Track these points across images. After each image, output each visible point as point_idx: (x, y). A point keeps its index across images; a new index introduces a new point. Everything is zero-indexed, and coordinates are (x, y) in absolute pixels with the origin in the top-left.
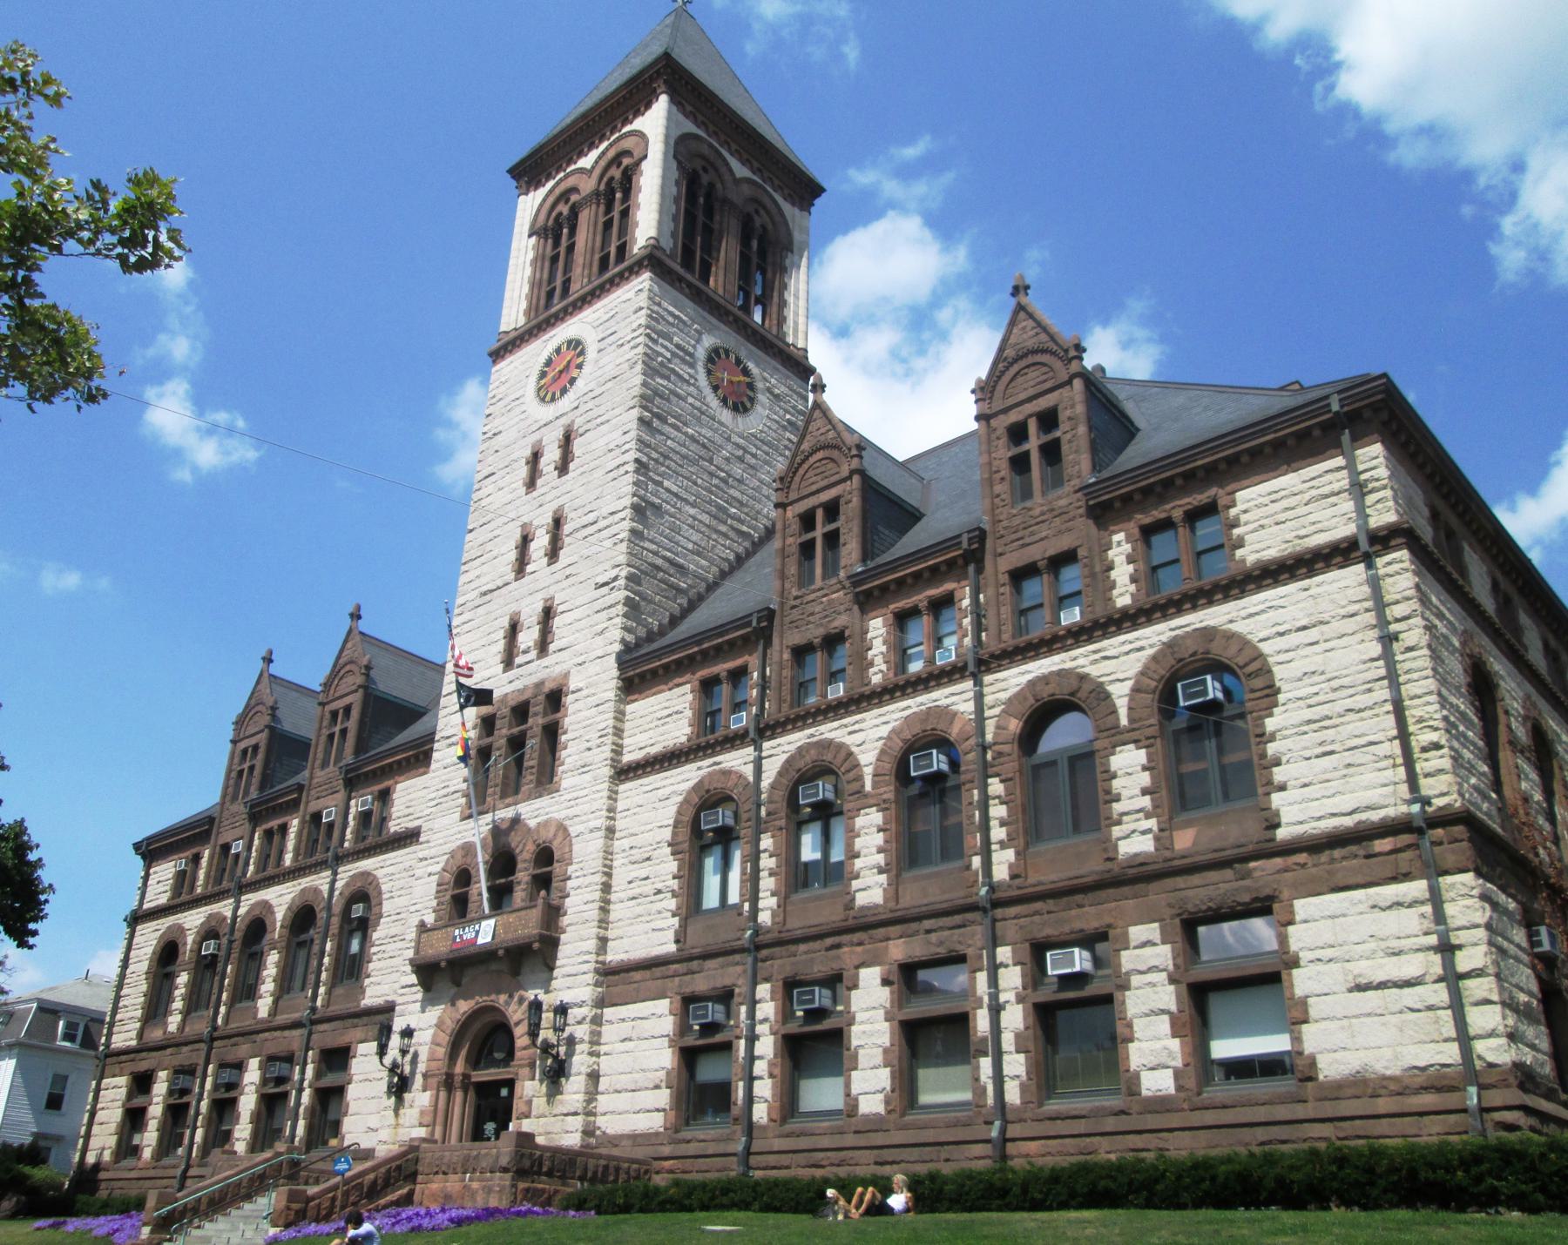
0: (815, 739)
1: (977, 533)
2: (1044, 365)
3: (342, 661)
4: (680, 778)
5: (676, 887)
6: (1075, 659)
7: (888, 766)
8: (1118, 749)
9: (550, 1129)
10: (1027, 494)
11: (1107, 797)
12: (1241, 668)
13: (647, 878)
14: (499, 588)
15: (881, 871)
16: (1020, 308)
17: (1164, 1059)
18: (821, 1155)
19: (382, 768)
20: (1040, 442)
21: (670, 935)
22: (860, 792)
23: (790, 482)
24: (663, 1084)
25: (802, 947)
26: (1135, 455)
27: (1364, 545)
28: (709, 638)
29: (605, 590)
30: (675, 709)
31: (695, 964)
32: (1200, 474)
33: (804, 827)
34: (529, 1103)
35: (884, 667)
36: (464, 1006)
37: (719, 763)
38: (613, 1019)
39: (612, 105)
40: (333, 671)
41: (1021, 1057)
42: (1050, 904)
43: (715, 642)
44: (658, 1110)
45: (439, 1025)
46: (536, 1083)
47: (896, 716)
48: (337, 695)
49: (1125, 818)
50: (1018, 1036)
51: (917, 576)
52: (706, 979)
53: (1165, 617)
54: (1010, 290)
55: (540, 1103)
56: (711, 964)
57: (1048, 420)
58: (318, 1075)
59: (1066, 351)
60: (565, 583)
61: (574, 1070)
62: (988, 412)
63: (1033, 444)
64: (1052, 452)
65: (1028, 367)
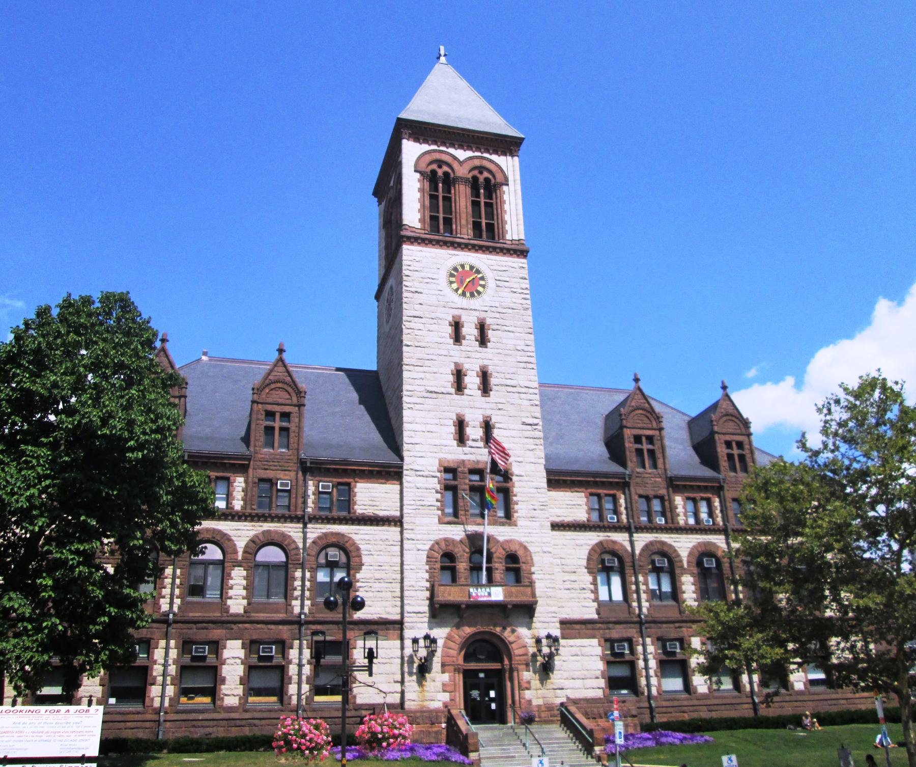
2: (287, 391)
3: (271, 377)
7: (694, 561)
8: (236, 568)
9: (546, 696)
13: (576, 581)
14: (443, 393)
15: (244, 598)
17: (801, 679)
18: (686, 708)
21: (594, 611)
22: (682, 567)
25: (665, 625)
28: (600, 477)
29: (529, 427)
31: (611, 625)
32: (227, 465)
34: (529, 682)
35: (313, 506)
36: (468, 630)
38: (565, 644)
44: (599, 688)
45: (449, 638)
51: (699, 487)
52: (617, 632)
53: (652, 532)
55: (535, 683)
56: (618, 626)
59: (301, 392)
61: (556, 668)
65: (280, 388)
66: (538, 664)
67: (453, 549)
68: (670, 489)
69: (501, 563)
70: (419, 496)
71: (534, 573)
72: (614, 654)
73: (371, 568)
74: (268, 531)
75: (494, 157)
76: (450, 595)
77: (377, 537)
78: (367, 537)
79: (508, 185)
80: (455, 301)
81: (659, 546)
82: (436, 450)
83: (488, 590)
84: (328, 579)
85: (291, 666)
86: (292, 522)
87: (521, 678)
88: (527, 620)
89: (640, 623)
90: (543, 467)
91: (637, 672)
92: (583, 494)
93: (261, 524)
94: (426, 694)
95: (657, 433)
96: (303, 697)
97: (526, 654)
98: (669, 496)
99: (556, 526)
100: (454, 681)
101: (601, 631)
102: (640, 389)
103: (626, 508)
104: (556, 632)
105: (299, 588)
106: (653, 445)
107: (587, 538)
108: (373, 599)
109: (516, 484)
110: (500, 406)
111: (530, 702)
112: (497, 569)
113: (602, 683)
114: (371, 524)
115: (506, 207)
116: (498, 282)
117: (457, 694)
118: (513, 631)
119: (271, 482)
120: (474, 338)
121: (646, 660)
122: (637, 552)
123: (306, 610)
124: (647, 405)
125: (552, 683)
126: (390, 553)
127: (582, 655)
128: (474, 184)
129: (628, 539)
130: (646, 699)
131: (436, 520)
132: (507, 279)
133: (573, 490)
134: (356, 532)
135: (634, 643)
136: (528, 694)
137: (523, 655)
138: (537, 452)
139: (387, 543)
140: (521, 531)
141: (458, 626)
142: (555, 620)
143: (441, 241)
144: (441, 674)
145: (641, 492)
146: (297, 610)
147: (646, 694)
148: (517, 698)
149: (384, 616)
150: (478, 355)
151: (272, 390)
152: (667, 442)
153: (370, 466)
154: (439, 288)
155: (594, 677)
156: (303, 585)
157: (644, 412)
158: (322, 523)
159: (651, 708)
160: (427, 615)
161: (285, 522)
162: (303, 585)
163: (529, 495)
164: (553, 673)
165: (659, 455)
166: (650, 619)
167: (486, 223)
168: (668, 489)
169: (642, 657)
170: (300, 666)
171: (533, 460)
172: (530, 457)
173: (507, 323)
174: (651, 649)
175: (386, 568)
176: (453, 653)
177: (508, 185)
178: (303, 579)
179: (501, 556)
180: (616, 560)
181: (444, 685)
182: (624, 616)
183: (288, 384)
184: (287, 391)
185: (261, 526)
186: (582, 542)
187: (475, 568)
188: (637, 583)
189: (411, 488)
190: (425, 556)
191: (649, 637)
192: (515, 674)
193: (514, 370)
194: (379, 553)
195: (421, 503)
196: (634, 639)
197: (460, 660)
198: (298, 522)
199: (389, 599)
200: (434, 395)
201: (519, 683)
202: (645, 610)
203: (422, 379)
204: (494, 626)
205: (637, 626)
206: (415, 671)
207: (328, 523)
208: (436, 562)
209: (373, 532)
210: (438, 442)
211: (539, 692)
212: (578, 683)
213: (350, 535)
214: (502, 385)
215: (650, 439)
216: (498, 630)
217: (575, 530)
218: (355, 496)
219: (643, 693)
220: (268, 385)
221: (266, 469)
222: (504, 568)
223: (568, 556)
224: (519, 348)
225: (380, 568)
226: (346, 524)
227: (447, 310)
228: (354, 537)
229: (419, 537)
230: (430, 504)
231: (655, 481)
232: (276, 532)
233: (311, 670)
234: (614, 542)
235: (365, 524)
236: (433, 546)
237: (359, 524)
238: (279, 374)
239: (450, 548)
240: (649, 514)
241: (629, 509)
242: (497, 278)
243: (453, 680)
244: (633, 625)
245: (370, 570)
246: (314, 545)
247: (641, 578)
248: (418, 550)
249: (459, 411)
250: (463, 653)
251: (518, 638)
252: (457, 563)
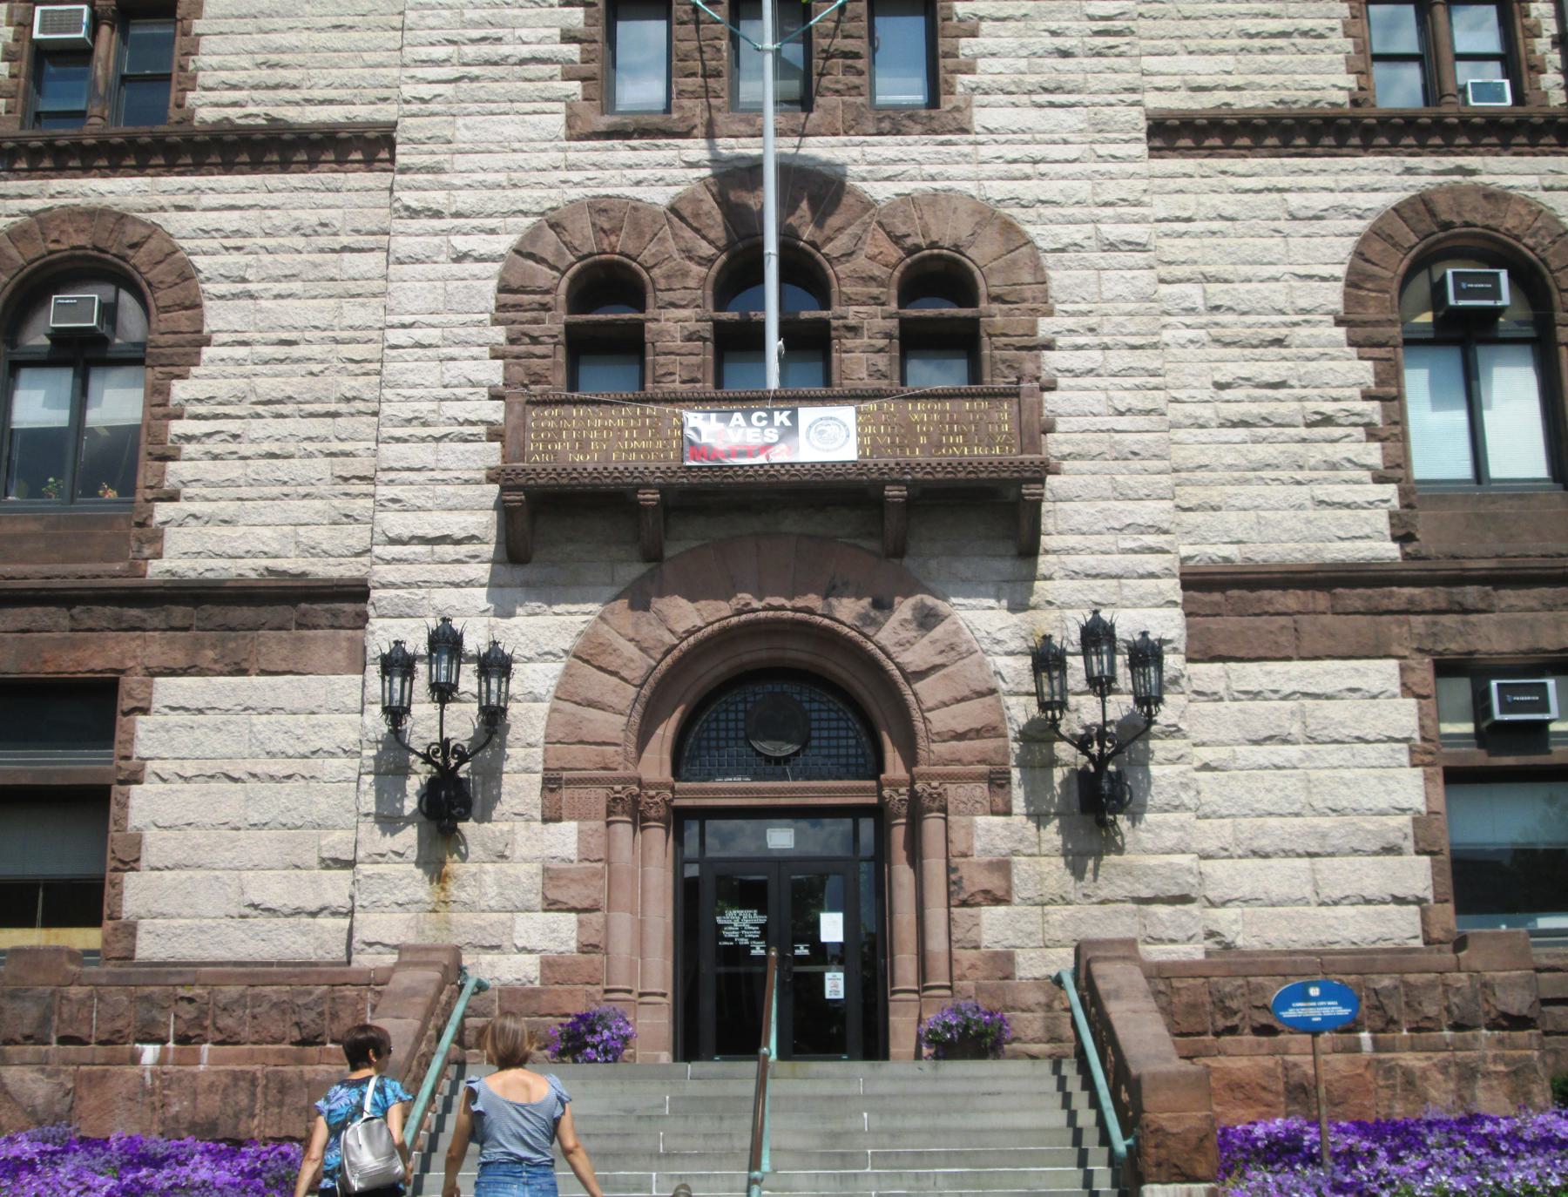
4: (1348, 180)
5: (1377, 418)
6: (638, 183)
12: (648, 270)
21: (1380, 519)
24: (1409, 845)
30: (1307, 24)
31: (1471, 594)
37: (1473, 172)
44: (1400, 901)
49: (1066, 465)
56: (1509, 596)
209: (262, 198)
228: (174, 223)
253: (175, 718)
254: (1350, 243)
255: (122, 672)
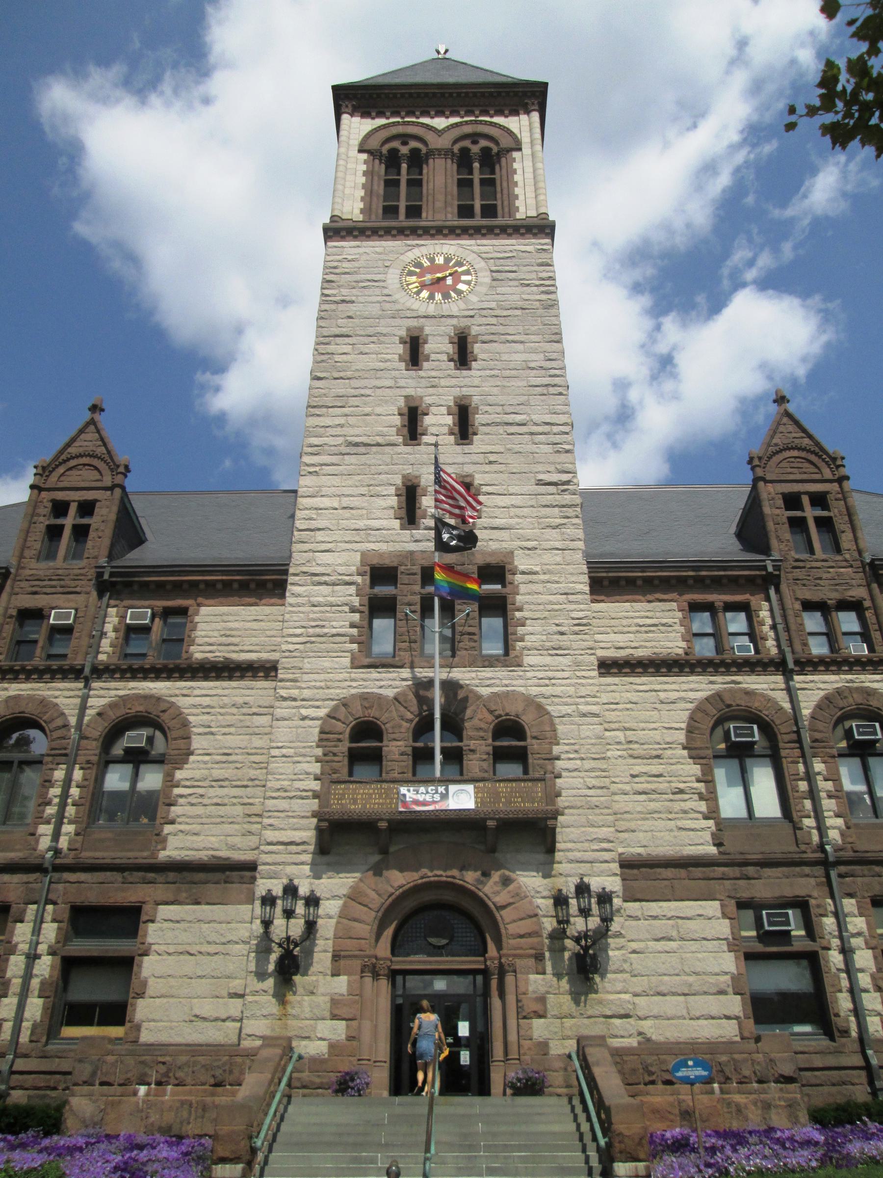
0: (855, 685)
1: (3, 571)
2: (96, 468)
3: (72, 450)
10: (51, 555)
11: (167, 801)
12: (384, 724)
14: (379, 445)
16: (92, 422)
19: (206, 583)
20: (75, 523)
23: (51, 472)
24: (730, 990)
26: (136, 557)
27: (87, 671)
28: (709, 568)
31: (751, 870)
32: (185, 586)
33: (111, 766)
34: (542, 1000)
35: (109, 650)
37: (739, 683)
39: (467, 93)
40: (57, 457)
41: (40, 1002)
42: (117, 876)
43: (716, 573)
44: (728, 1018)
45: (354, 896)
46: (549, 977)
47: (113, 693)
48: (61, 485)
49: (566, 811)
50: (42, 983)
54: (90, 405)
56: (768, 872)
57: (87, 508)
58: (64, 938)
59: (118, 466)
60: (487, 468)
61: (612, 966)
62: (42, 486)
63: (69, 521)
64: (81, 533)
65: (85, 465)
66: (567, 955)
67: (377, 715)
68: (875, 586)
69: (483, 738)
70: (314, 620)
71: (558, 758)
72: (764, 937)
73: (207, 758)
74: (17, 698)
75: (499, 120)
76: (355, 802)
77: (226, 700)
78: (206, 701)
79: (520, 149)
80: (414, 307)
81: (858, 698)
82: (357, 539)
83: (441, 789)
84: (125, 786)
85: (13, 958)
86: (64, 678)
87: (522, 989)
88: (541, 857)
89: (826, 864)
90: (579, 556)
91: (827, 980)
92: (674, 605)
93: (6, 685)
94: (292, 1023)
95: (835, 486)
96: (26, 1025)
97: (536, 934)
98: (873, 599)
99: (607, 667)
100: (360, 995)
101: (727, 883)
102: (788, 414)
103: (774, 627)
104: (613, 884)
105: (56, 800)
106: (829, 510)
107: (685, 687)
108: (204, 820)
109: (523, 588)
110: (492, 458)
111: (544, 1046)
112: (473, 751)
113: (735, 1005)
114: (218, 678)
115: (517, 178)
116: (494, 274)
117: (367, 1025)
118: (506, 882)
119: (37, 615)
120: (445, 357)
121: (846, 951)
122: (806, 712)
123: (63, 843)
124: (807, 441)
125: (600, 1002)
126: (250, 731)
127: (682, 939)
128: (464, 160)
129: (783, 686)
130: (856, 1046)
131: (346, 661)
132: (514, 269)
133: (650, 597)
134: (185, 692)
135: (814, 911)
136: (539, 1028)
137: (529, 935)
138: (570, 531)
139: (245, 710)
140: (529, 674)
141: (378, 870)
142: (607, 856)
143: (394, 228)
144: (329, 978)
145: (808, 595)
146: (45, 843)
147: (854, 1034)
148: (512, 1037)
149: (224, 853)
150: (454, 382)
151: (70, 469)
152: (857, 501)
153: (223, 573)
154: (386, 292)
155: (714, 990)
156: (65, 795)
157: (803, 454)
158: (122, 678)
159: (868, 1067)
160: (311, 848)
161: (53, 679)
162: (65, 795)
163: (550, 607)
164: (603, 976)
165: (841, 524)
166: (848, 854)
167: (482, 206)
168: (868, 585)
169: (836, 942)
170: (32, 957)
171: (558, 545)
172: (553, 538)
173: (510, 330)
174: (857, 923)
175: (239, 758)
176: (365, 930)
177: (520, 149)
178: (67, 783)
179: (483, 725)
180: (755, 727)
181: (334, 1002)
182: (783, 846)
183: (99, 458)
184: (96, 468)
185: (6, 689)
186: (674, 695)
187: (423, 756)
188: (809, 777)
189: (298, 605)
190: (317, 730)
191: (850, 895)
192: (509, 979)
193: (523, 399)
194: (226, 730)
195: (318, 631)
196: (812, 902)
197: (384, 948)
198: (77, 679)
199: (239, 819)
200: (362, 449)
201: (518, 1001)
202: (834, 835)
203: (341, 426)
204: (463, 868)
205: (819, 870)
206: (271, 967)
207: (134, 678)
208: (339, 740)
210: (361, 524)
211: (568, 1022)
212: (672, 1005)
213: (173, 699)
214: (497, 424)
215: (819, 500)
216: (470, 877)
217: (657, 673)
218: (194, 629)
219: (846, 1032)
220: (65, 461)
221: (35, 593)
222: (490, 749)
223: (642, 725)
224: (532, 365)
225: (224, 758)
226: (168, 678)
227: (398, 321)
228: (182, 702)
229: (307, 693)
230: (334, 631)
231: (839, 575)
232: (31, 698)
233: (52, 967)
234: (748, 693)
235: (206, 678)
236: (335, 709)
237: (193, 678)
238: (86, 443)
239: (373, 713)
240: (831, 636)
241: (780, 627)
242: (494, 268)
243: (356, 992)
244: (807, 870)
245: (205, 763)
246: (99, 719)
247: (819, 766)
248: (304, 718)
249: (408, 470)
250: (389, 932)
251: (519, 896)
252: (385, 743)
253: (166, 925)
254: (687, 713)
255: (144, 903)
